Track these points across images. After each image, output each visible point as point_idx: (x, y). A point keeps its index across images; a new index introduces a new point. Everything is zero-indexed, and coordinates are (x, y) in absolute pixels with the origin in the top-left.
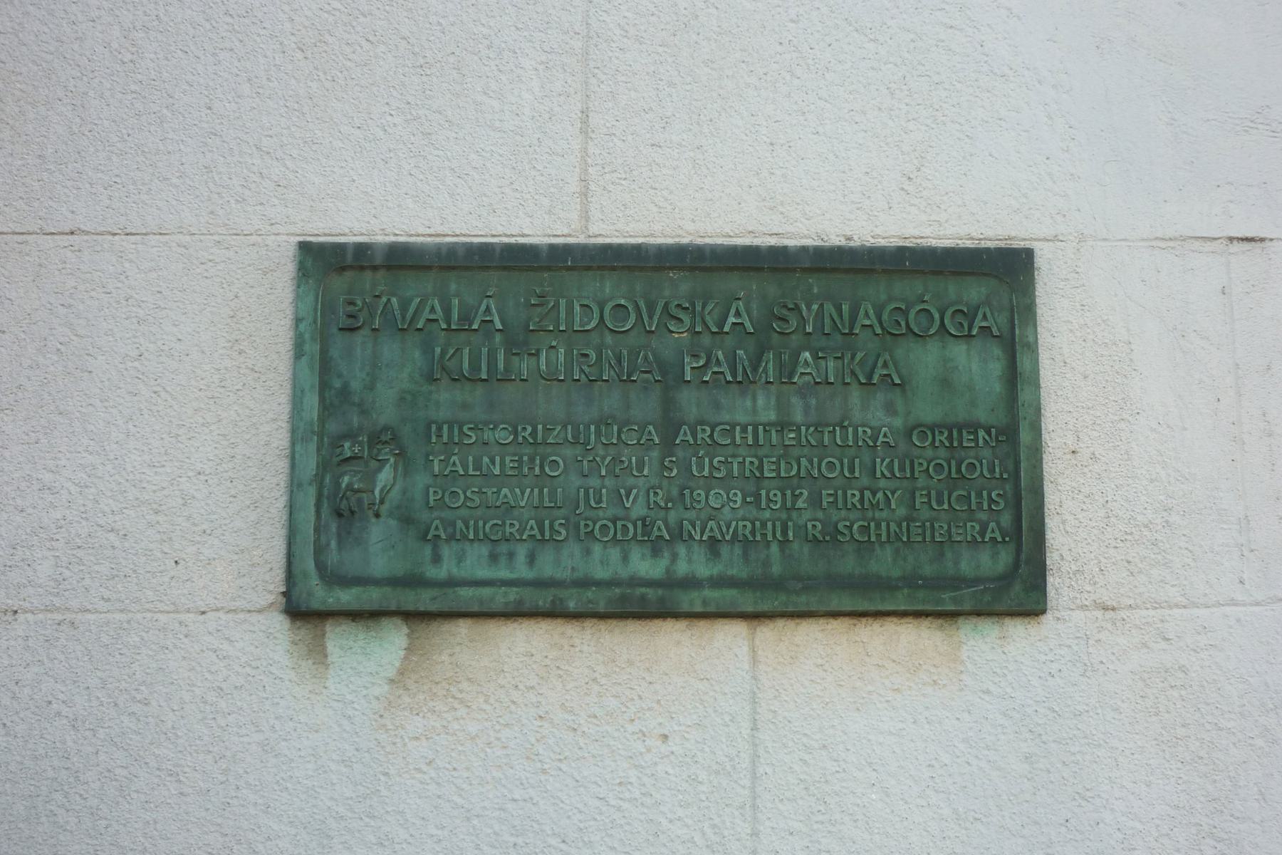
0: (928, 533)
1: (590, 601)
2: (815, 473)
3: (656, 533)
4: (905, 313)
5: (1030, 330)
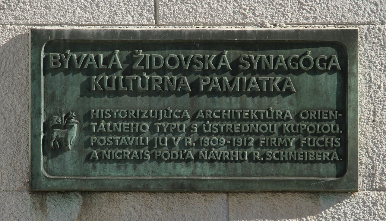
0: (306, 156)
1: (160, 185)
2: (257, 131)
3: (188, 156)
4: (298, 61)
5: (355, 67)
